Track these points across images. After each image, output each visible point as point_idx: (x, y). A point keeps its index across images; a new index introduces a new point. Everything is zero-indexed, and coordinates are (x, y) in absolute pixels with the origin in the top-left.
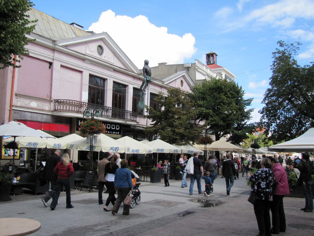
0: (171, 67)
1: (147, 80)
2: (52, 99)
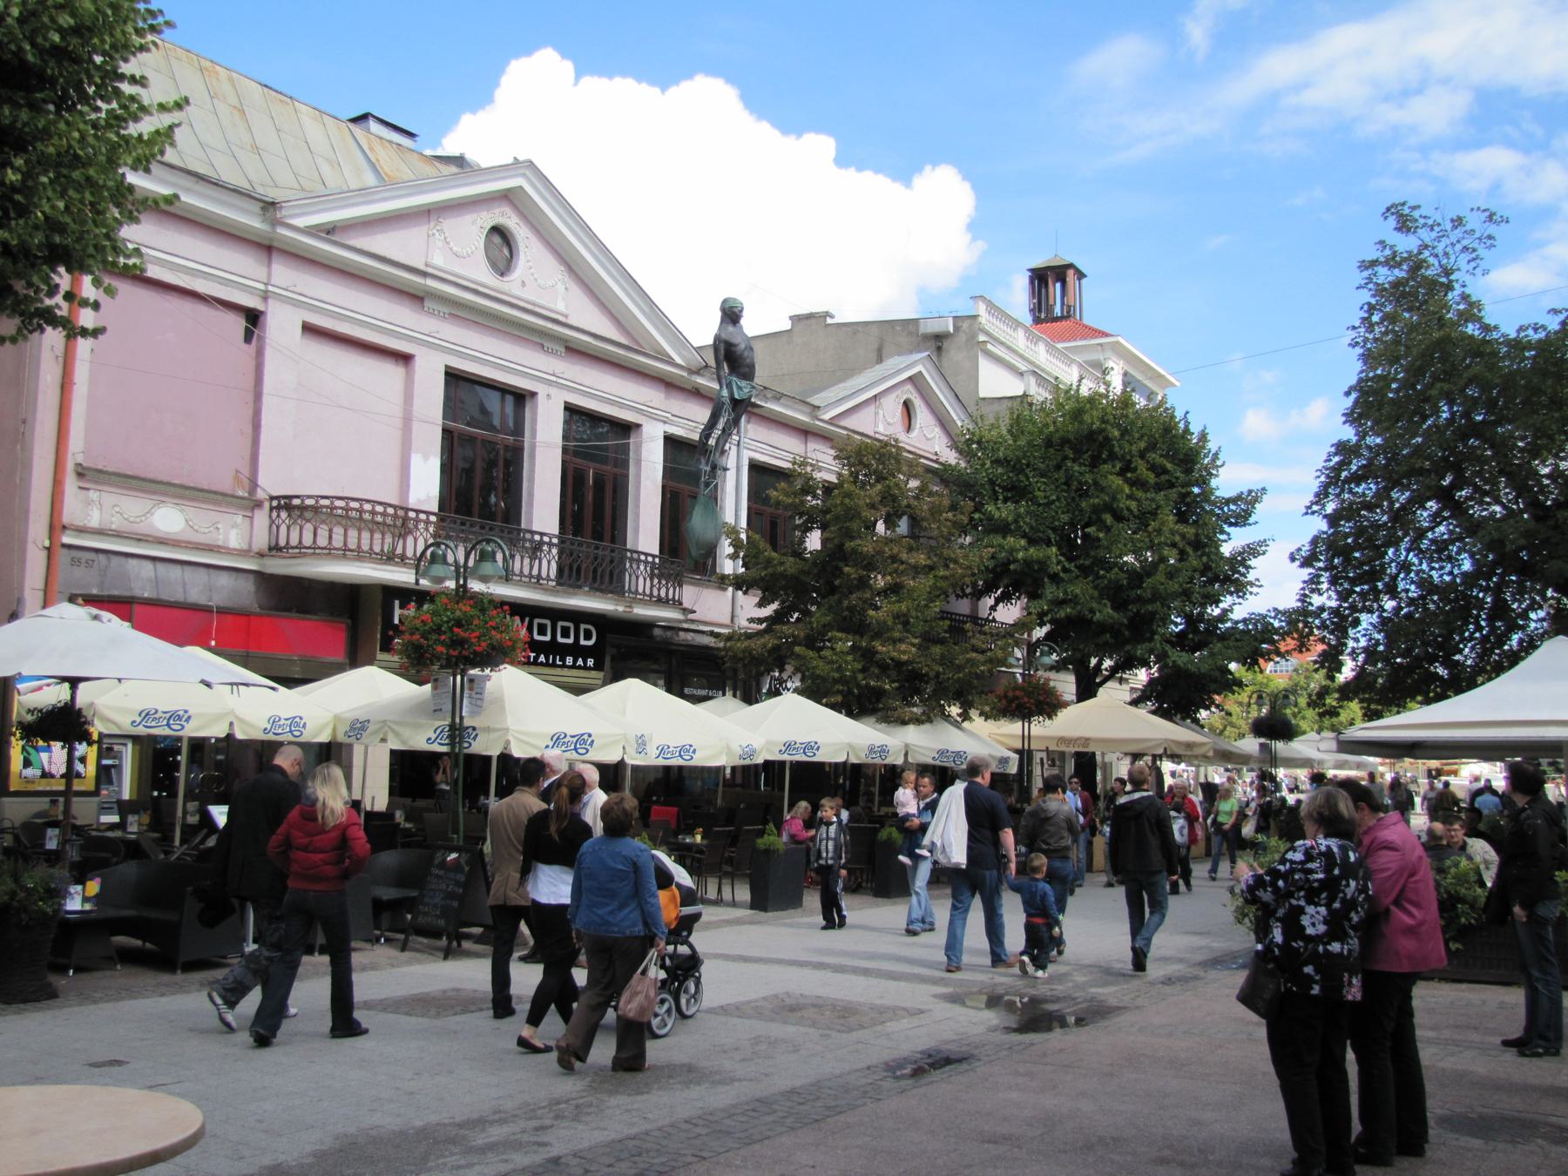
0: (854, 333)
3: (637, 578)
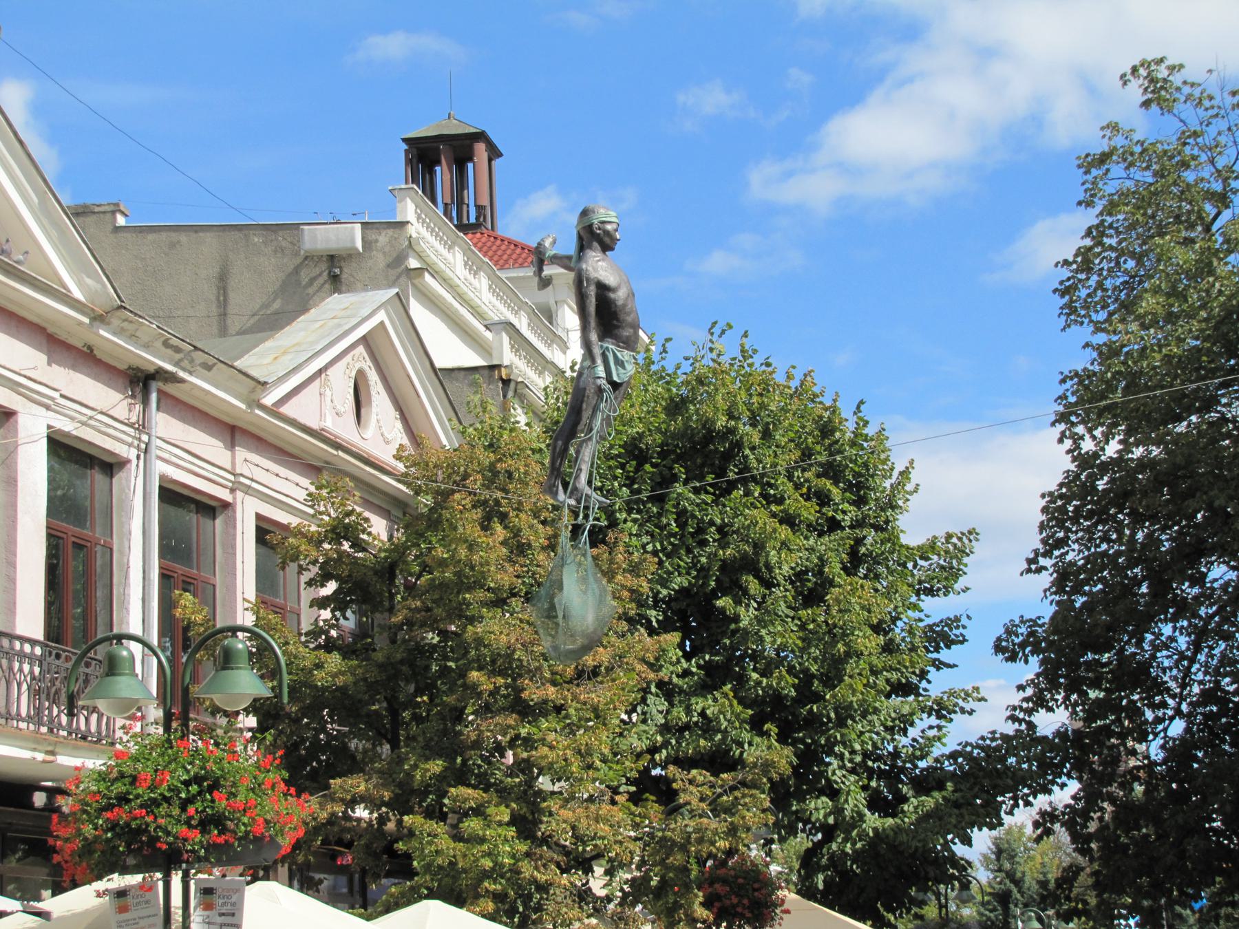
0: (173, 245)
1: (615, 378)
2: (239, 494)
3: (19, 685)
